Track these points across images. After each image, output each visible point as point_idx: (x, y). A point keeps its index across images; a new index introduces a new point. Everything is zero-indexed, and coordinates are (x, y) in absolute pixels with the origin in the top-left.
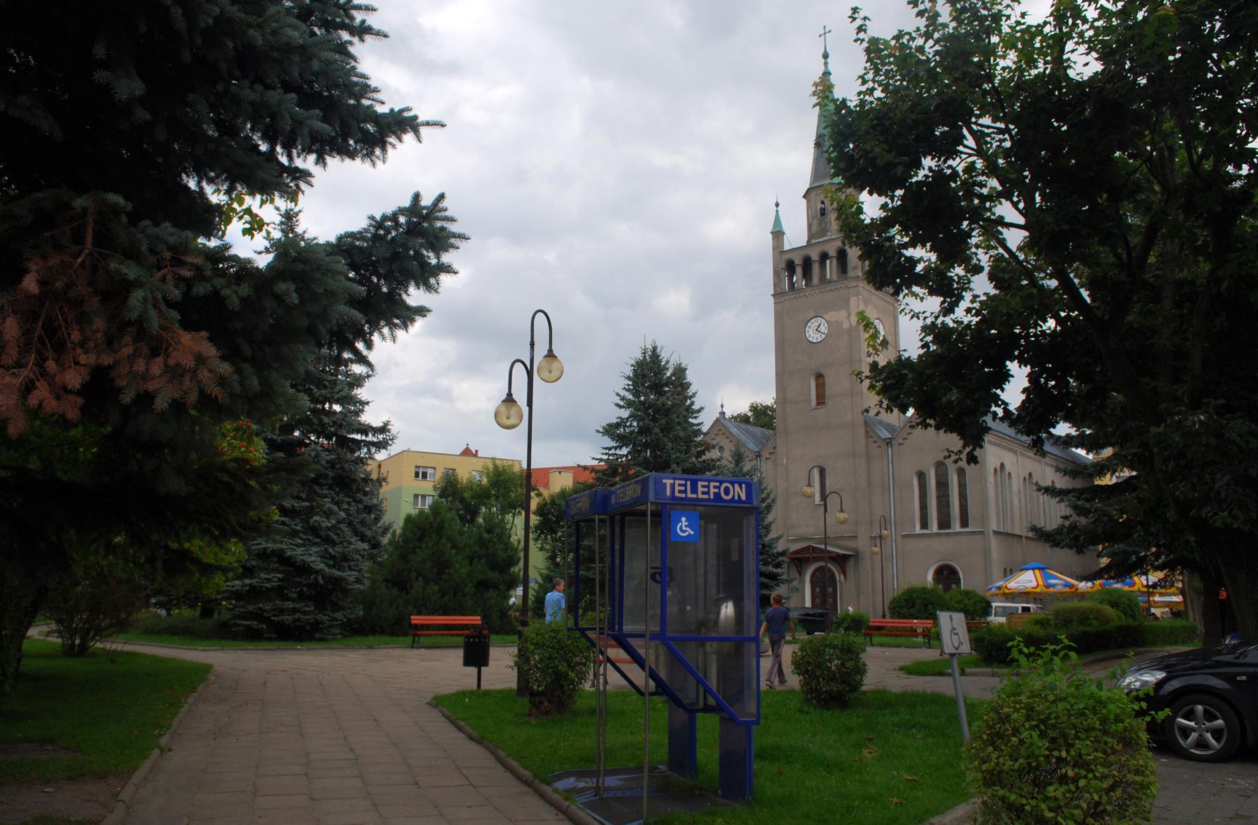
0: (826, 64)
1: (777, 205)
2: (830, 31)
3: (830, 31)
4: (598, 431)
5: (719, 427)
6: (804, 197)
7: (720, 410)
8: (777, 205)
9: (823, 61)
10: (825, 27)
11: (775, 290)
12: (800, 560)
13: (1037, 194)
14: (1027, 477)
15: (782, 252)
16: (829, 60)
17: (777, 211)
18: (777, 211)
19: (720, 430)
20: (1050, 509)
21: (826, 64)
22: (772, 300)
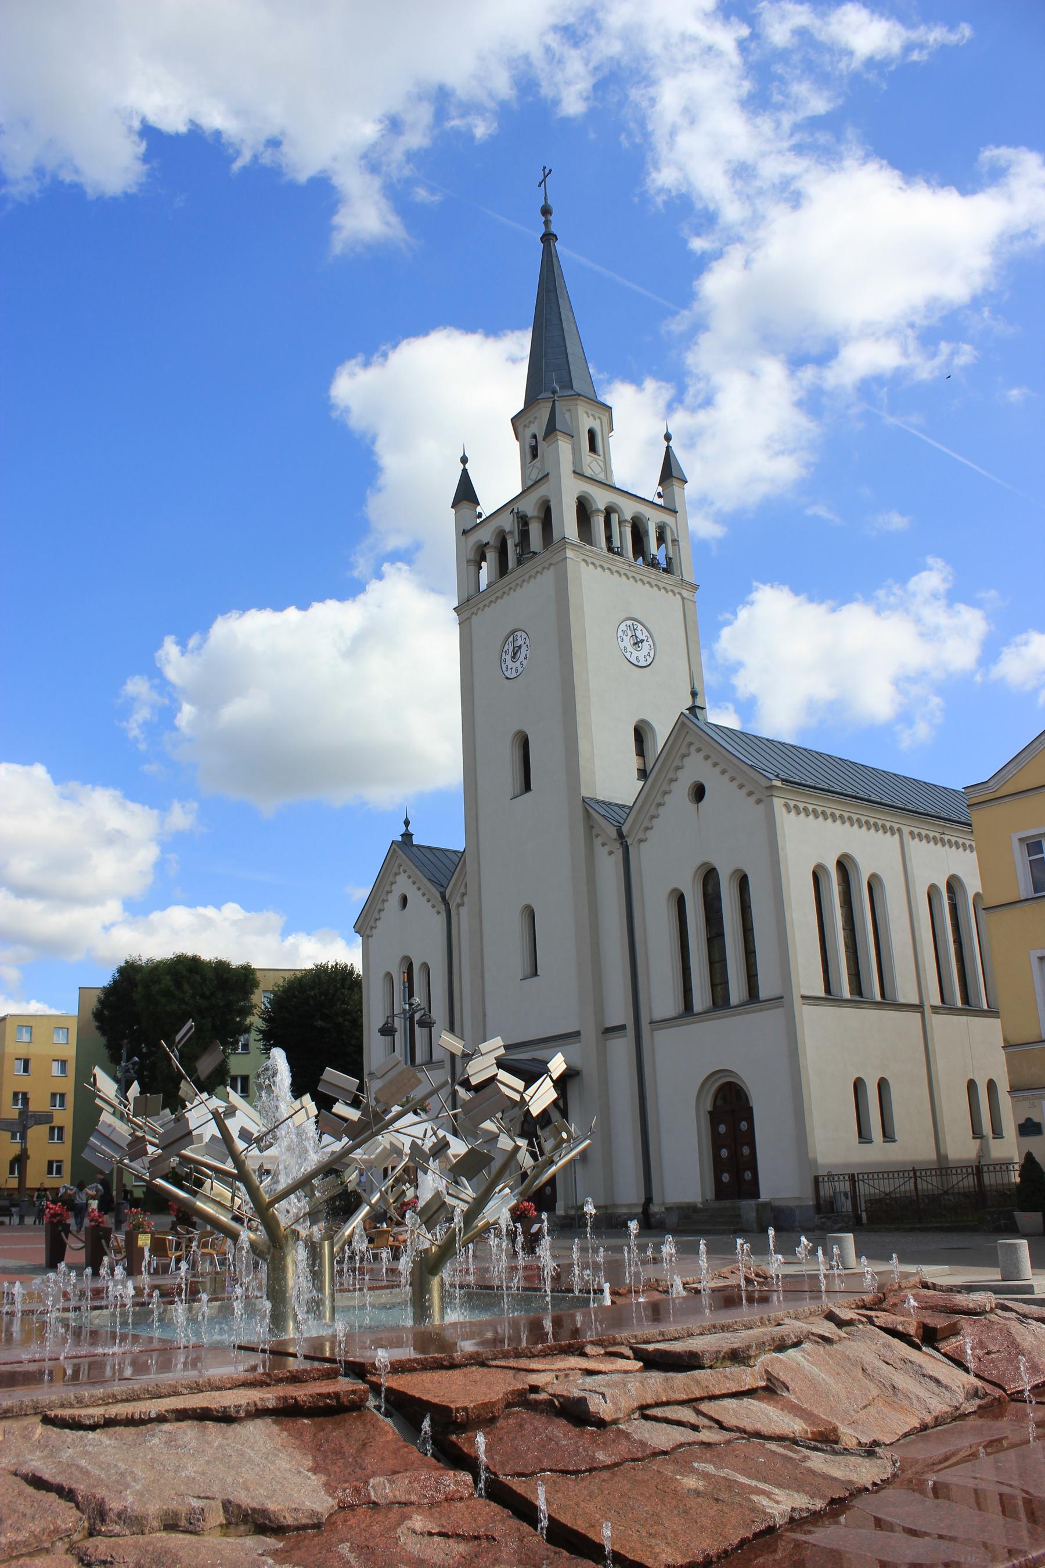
0: (547, 223)
3: (539, 186)
5: (688, 739)
10: (545, 168)
21: (547, 223)
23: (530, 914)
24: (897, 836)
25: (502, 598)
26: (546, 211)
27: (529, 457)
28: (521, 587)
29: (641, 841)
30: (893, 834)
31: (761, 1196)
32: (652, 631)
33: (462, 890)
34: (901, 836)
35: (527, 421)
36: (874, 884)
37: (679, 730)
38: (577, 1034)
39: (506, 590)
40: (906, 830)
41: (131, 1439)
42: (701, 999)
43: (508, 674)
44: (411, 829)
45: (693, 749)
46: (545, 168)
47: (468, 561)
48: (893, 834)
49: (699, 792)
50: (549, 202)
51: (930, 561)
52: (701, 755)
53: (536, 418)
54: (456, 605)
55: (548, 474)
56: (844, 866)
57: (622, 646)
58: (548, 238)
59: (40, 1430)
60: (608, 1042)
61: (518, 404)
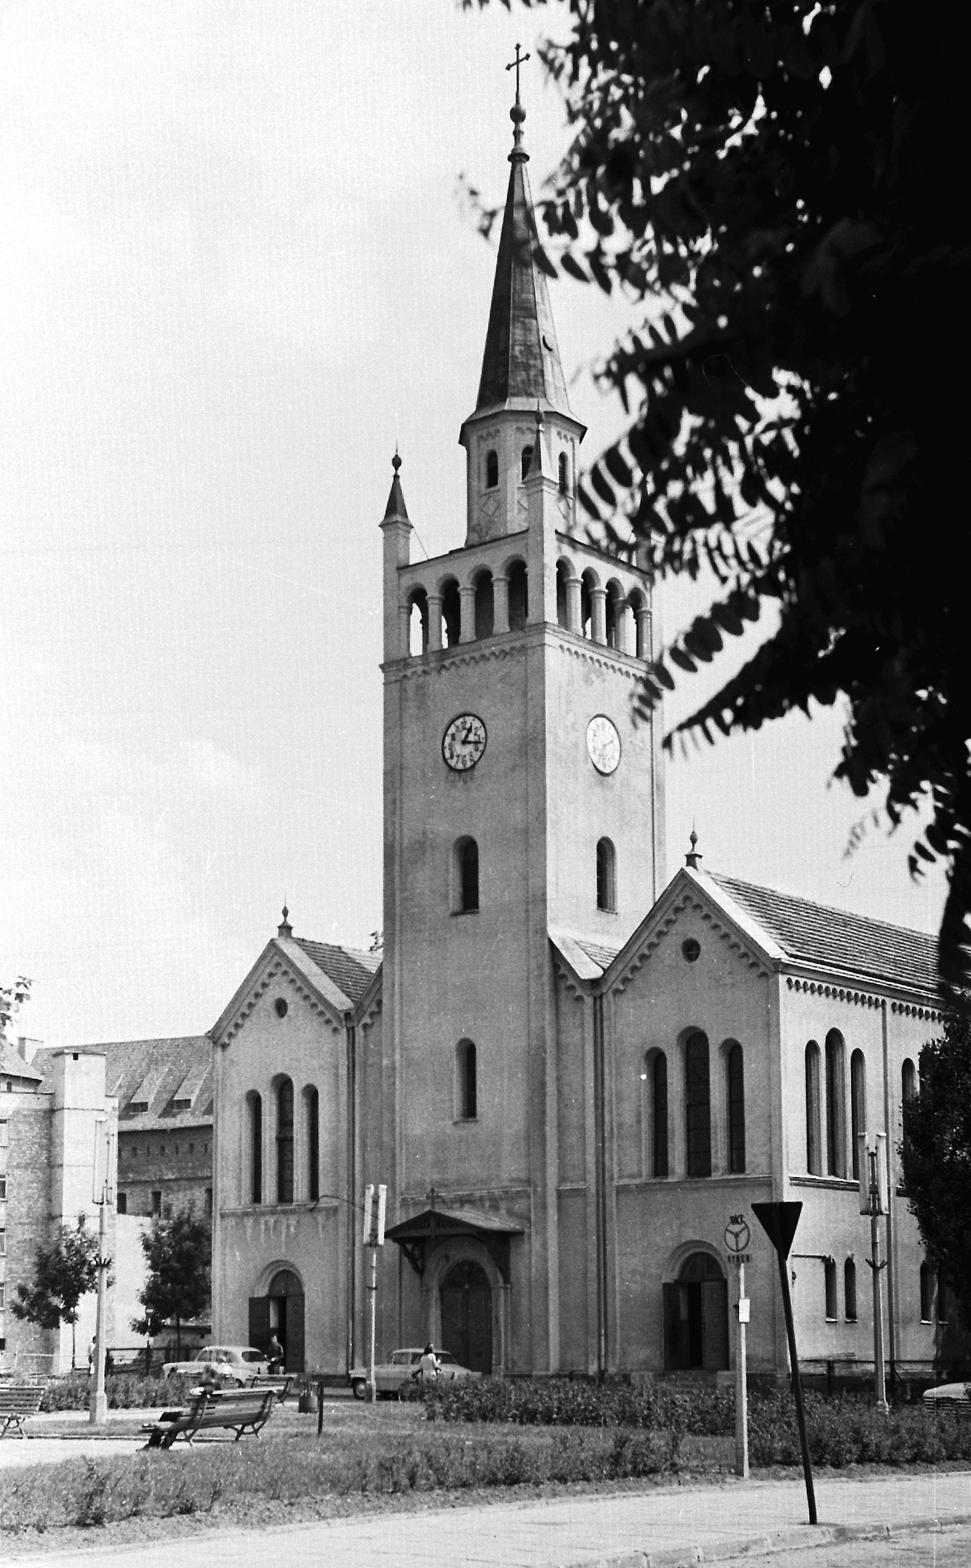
0: (517, 134)
1: (397, 462)
2: (508, 68)
3: (508, 68)
4: (700, 857)
5: (687, 892)
6: (460, 442)
7: (281, 920)
8: (397, 462)
9: (512, 125)
10: (518, 47)
11: (386, 656)
12: (419, 1241)
13: (796, 453)
14: (822, 1044)
15: (404, 568)
16: (523, 126)
17: (396, 477)
18: (396, 477)
19: (687, 898)
20: (612, 1129)
21: (517, 134)
22: (380, 677)
24: (880, 1009)
27: (481, 484)
30: (876, 1007)
32: (615, 722)
33: (374, 1008)
34: (884, 1009)
36: (858, 1056)
40: (889, 1002)
41: (837, 1401)
44: (290, 921)
46: (518, 47)
48: (876, 1007)
51: (731, 112)
54: (382, 662)
56: (834, 1038)
59: (161, 1522)
61: (468, 406)
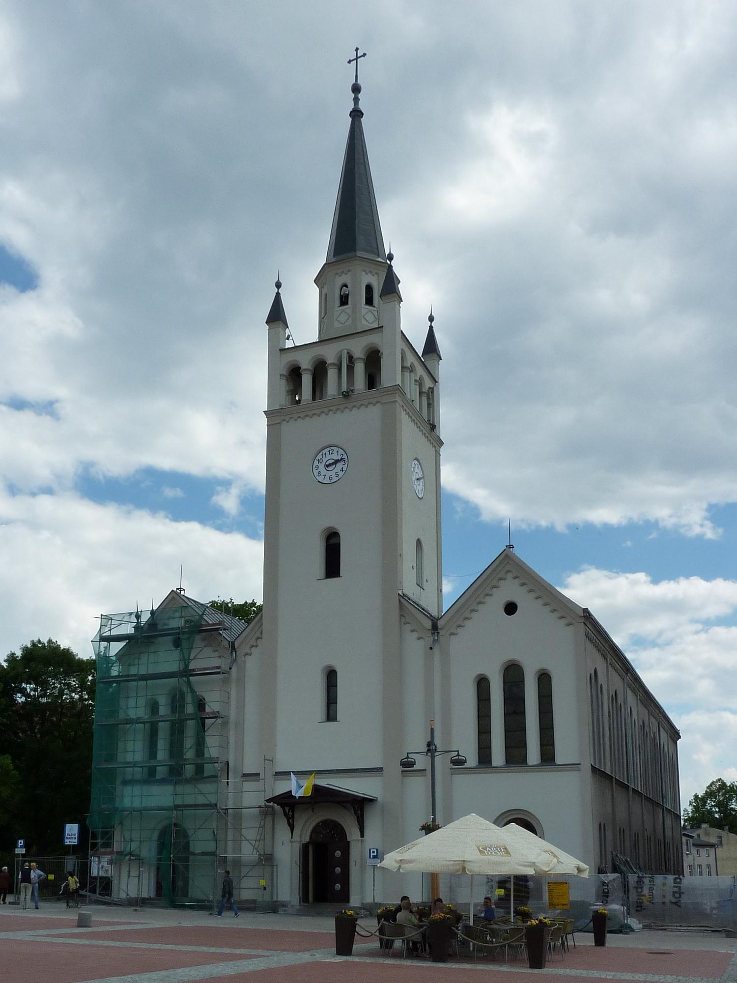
0: (356, 100)
10: (357, 49)
21: (356, 100)
23: (331, 676)
25: (319, 416)
26: (356, 89)
28: (342, 412)
29: (452, 634)
31: (351, 900)
35: (341, 271)
37: (503, 559)
38: (258, 775)
39: (326, 410)
42: (498, 754)
43: (321, 479)
45: (509, 575)
46: (357, 49)
47: (281, 375)
49: (511, 608)
50: (359, 82)
52: (517, 581)
53: (349, 271)
55: (382, 327)
57: (341, 474)
58: (356, 114)
60: (278, 782)
